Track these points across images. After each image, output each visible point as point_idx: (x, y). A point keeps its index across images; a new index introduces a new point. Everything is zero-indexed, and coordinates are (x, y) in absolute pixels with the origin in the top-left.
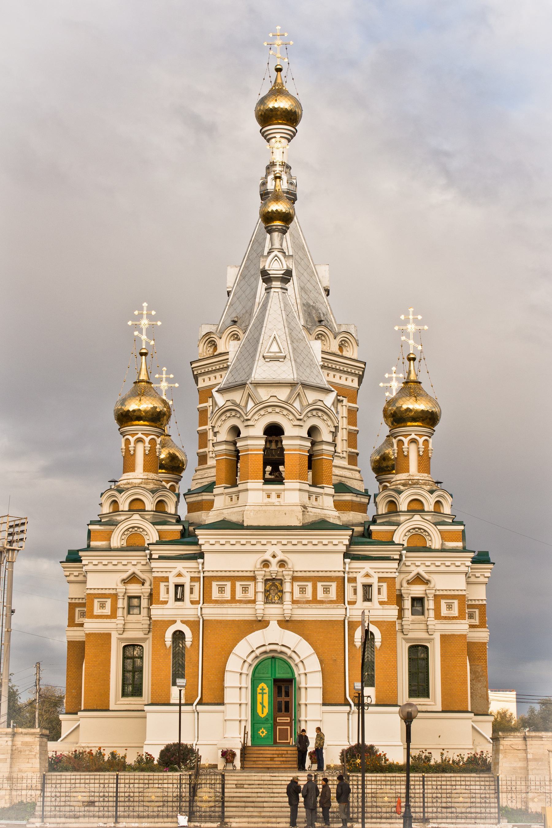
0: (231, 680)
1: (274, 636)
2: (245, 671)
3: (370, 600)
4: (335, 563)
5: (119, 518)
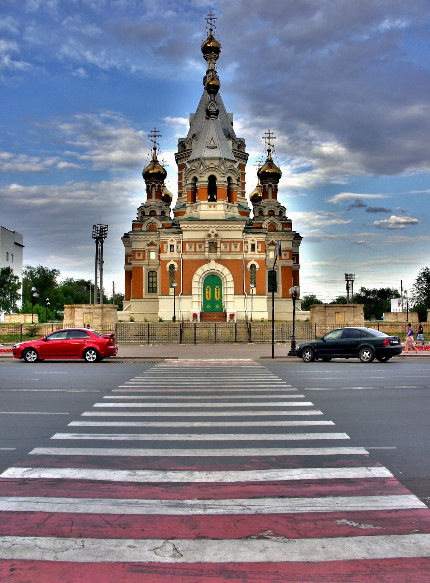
0: (195, 285)
1: (213, 266)
2: (201, 281)
3: (254, 251)
4: (239, 235)
5: (145, 219)
